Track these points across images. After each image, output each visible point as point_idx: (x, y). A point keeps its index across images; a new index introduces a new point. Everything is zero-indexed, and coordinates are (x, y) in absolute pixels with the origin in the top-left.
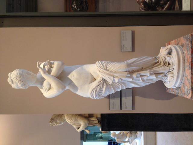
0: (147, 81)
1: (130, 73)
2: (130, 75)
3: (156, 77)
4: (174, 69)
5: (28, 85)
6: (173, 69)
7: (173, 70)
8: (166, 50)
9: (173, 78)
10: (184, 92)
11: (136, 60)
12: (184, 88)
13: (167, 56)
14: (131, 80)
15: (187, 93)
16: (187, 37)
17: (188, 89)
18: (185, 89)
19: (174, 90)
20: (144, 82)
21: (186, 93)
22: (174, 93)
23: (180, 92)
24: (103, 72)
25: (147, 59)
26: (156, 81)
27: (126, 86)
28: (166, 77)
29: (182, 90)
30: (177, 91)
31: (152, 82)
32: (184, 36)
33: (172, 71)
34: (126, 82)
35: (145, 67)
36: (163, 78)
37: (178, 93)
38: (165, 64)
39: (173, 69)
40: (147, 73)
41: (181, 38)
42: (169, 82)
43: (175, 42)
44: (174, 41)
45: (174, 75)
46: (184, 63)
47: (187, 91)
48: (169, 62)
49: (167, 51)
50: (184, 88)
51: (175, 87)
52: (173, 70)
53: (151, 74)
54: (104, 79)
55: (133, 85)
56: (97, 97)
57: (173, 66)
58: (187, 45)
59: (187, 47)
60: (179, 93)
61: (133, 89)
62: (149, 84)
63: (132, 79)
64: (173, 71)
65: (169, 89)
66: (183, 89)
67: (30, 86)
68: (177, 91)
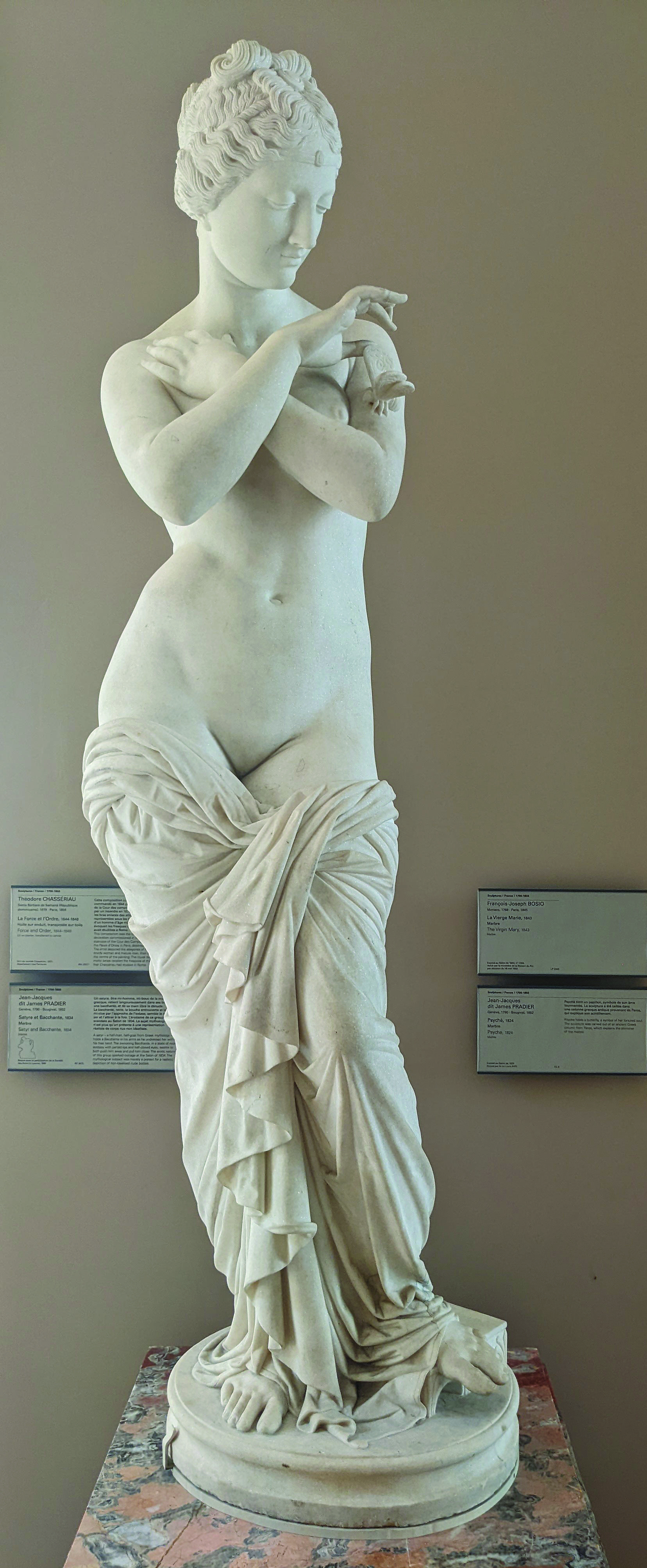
0: (223, 1207)
1: (291, 1063)
2: (275, 1068)
3: (255, 1284)
4: (322, 1434)
5: (202, 213)
6: (322, 1427)
7: (314, 1421)
8: (207, 161)
9: (245, 1419)
10: (127, 1518)
11: (403, 1129)
12: (158, 1516)
13: (427, 1377)
14: (236, 1071)
15: (111, 1545)
16: (582, 1552)
17: (147, 1549)
18: (146, 1528)
19: (150, 1423)
20: (214, 1180)
21: (115, 1536)
22: (131, 1416)
23: (132, 1471)
24: (300, 846)
25: (407, 1204)
26: (228, 1274)
27: (186, 1024)
28: (252, 1366)
29: (146, 1491)
30: (141, 1444)
31: (217, 1242)
32: (591, 1523)
33: (301, 1416)
34: (218, 1032)
35: (336, 1189)
36: (251, 1336)
37: (124, 1458)
38: (361, 1359)
39: (322, 1427)
40: (292, 1206)
41: (578, 1488)
42: (218, 1387)
43: (549, 1431)
44: (553, 1422)
45: (266, 1433)
46: (362, 1521)
47: (130, 1540)
48: (384, 1389)
49: (470, 1382)
50: (158, 1516)
51: (175, 1438)
52: (314, 1421)
53: (279, 1242)
54: (242, 850)
55: (192, 1082)
56: (98, 784)
57: (344, 1424)
58: (516, 1549)
59: (503, 1549)
60: (123, 1469)
61: (165, 1078)
62: (206, 1220)
63: (239, 1085)
64: (306, 1420)
65: (164, 1387)
66: (152, 1510)
67: (200, 231)
68: (141, 1444)
